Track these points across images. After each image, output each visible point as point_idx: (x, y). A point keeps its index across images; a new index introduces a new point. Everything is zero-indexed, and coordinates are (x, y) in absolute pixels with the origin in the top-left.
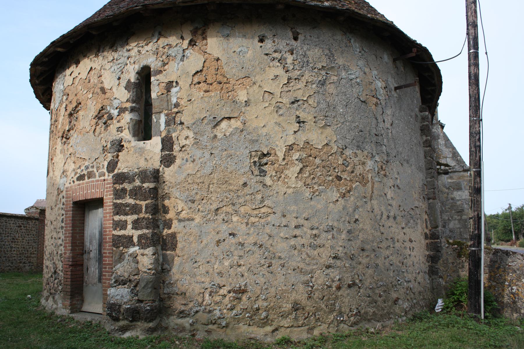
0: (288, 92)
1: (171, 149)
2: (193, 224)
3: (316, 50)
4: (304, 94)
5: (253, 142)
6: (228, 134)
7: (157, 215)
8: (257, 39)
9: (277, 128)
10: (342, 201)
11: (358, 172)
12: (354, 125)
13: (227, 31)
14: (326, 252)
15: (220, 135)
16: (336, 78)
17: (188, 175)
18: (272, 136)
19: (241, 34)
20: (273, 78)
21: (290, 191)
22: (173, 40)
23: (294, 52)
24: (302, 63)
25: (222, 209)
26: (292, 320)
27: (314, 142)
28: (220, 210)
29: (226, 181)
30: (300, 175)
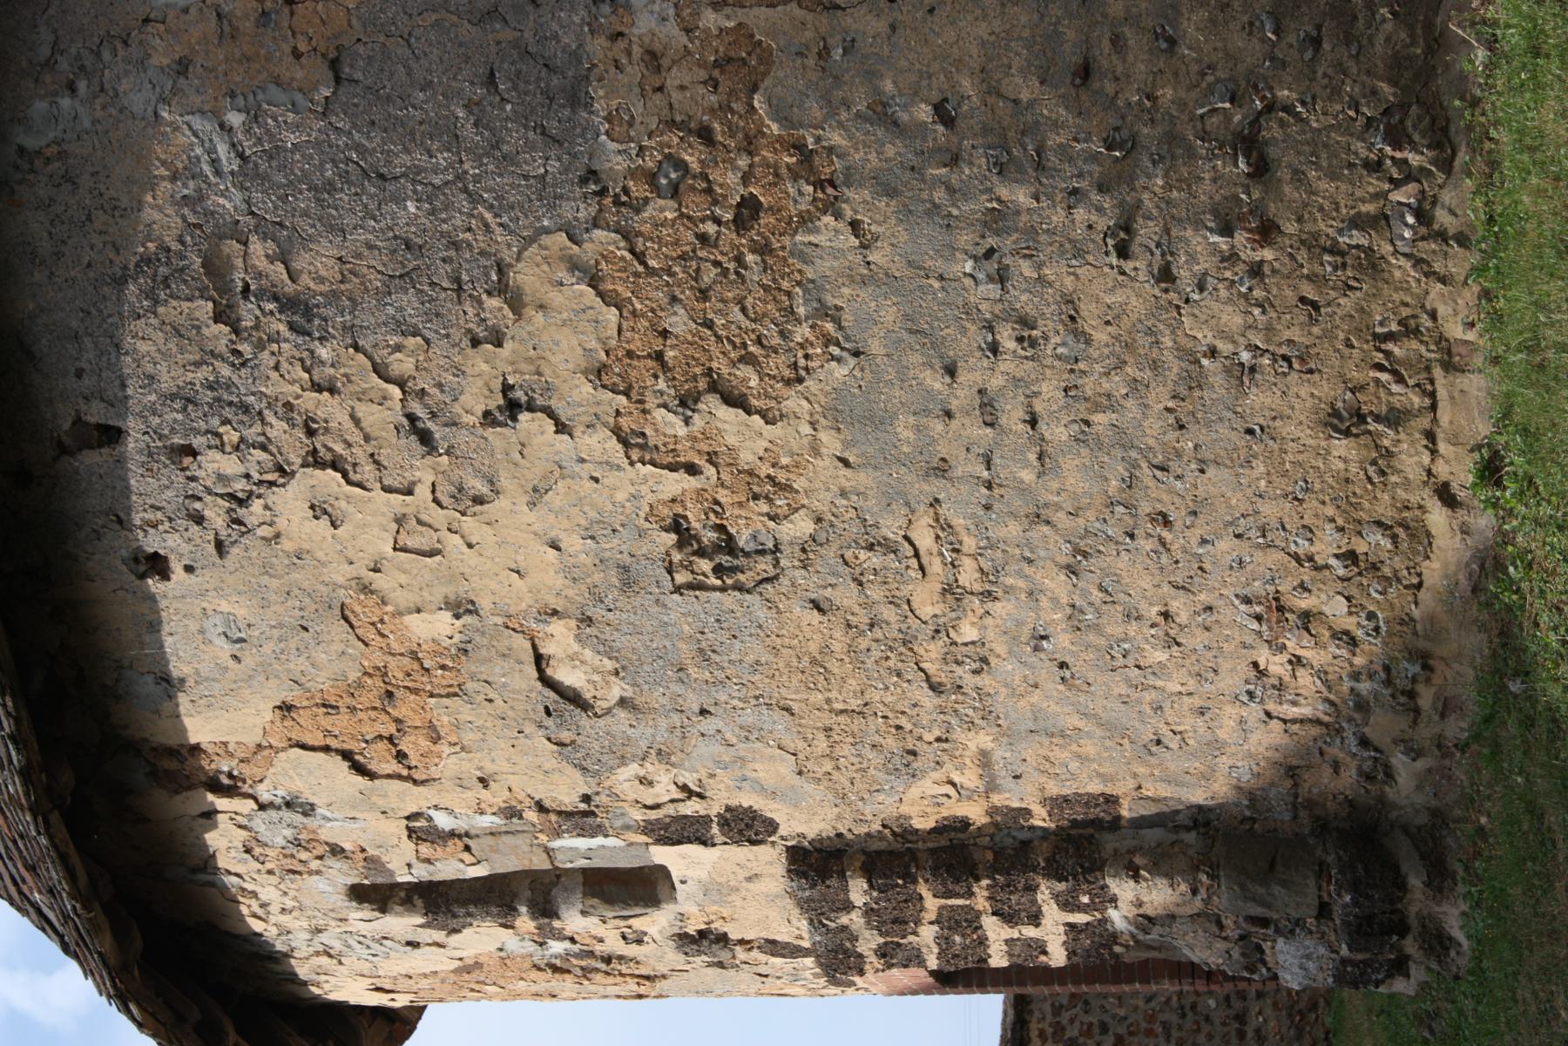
0: (377, 462)
1: (705, 820)
2: (1000, 754)
3: (143, 347)
4: (376, 396)
5: (628, 580)
6: (609, 665)
7: (977, 856)
8: (153, 584)
9: (555, 499)
10: (856, 199)
11: (699, 101)
12: (468, 131)
13: (147, 685)
14: (1095, 289)
15: (617, 690)
16: (257, 247)
17: (800, 773)
18: (593, 514)
19: (147, 638)
20: (324, 522)
21: (830, 442)
22: (223, 842)
23: (177, 440)
24: (228, 412)
25: (930, 672)
26: (1402, 436)
27: (593, 344)
28: (935, 680)
29: (814, 662)
30: (754, 402)
